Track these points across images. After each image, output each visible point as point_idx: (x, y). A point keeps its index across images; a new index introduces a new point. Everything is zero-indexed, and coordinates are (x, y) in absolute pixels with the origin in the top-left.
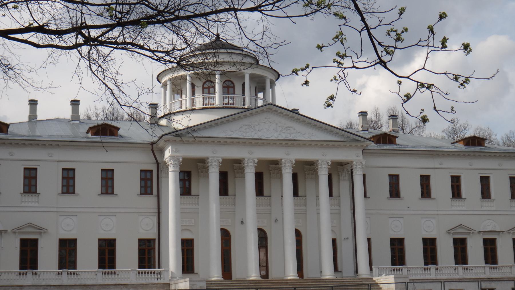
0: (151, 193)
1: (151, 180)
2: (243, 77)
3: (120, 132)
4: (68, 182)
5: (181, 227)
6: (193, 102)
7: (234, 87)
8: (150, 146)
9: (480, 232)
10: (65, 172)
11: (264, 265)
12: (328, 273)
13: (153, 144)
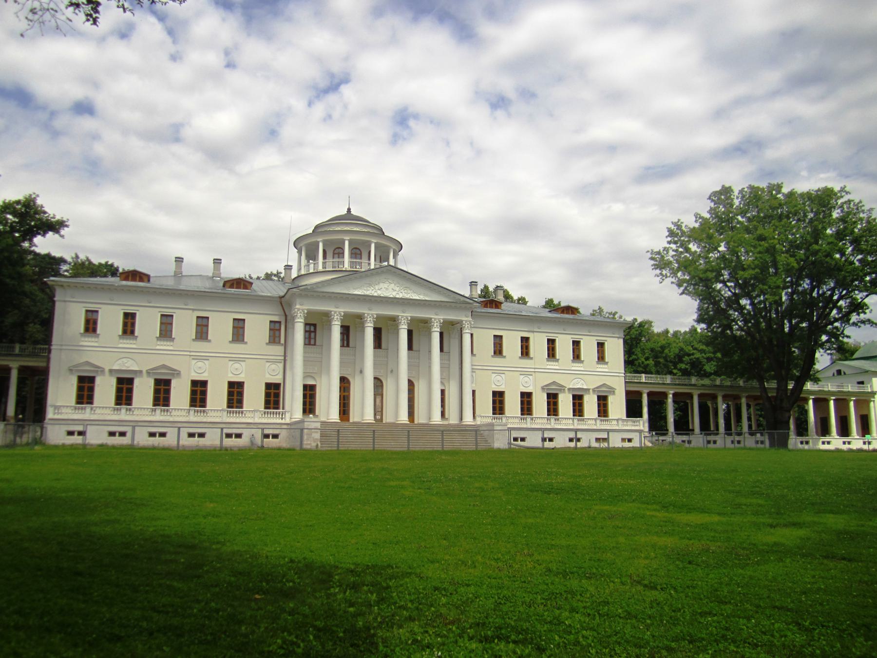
0: (279, 342)
1: (280, 330)
4: (274, 334)
7: (361, 254)
9: (569, 389)
10: (273, 324)
11: (378, 410)
12: (436, 418)
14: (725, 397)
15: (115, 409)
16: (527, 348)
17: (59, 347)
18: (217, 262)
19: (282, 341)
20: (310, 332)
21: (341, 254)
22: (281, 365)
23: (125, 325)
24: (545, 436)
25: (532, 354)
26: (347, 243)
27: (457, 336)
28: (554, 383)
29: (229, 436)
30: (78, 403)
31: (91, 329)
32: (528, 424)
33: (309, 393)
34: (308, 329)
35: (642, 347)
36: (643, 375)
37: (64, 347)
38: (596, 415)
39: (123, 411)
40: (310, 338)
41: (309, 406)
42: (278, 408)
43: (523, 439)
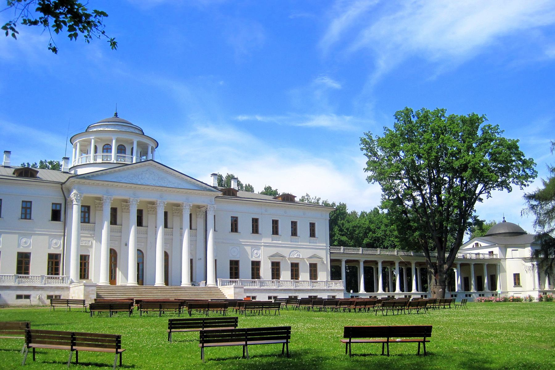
2: (132, 143)
3: (38, 175)
4: (26, 211)
5: (79, 246)
6: (95, 158)
7: (125, 150)
8: (60, 186)
10: (83, 208)
13: (62, 184)
16: (236, 225)
25: (239, 229)
26: (114, 141)
27: (203, 216)
33: (84, 261)
34: (24, 206)
35: (341, 225)
40: (26, 214)
41: (84, 273)
42: (58, 274)
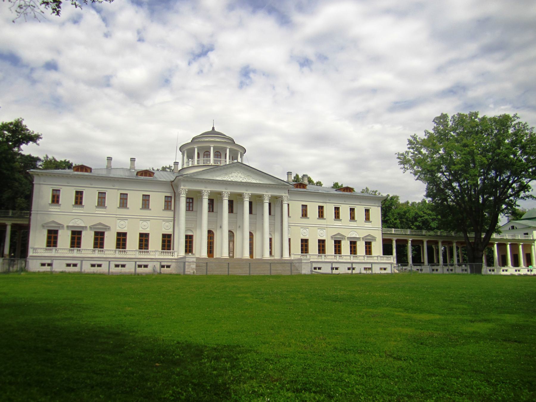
0: (171, 209)
1: (171, 202)
4: (168, 204)
7: (221, 155)
9: (348, 238)
10: (167, 198)
11: (231, 251)
12: (267, 256)
14: (443, 243)
15: (70, 250)
16: (322, 212)
17: (36, 212)
18: (133, 160)
19: (173, 208)
20: (189, 203)
21: (208, 155)
22: (172, 223)
23: (76, 198)
24: (333, 266)
25: (325, 216)
26: (212, 148)
27: (280, 205)
28: (339, 234)
29: (140, 266)
30: (48, 246)
31: (55, 201)
32: (323, 259)
33: (189, 240)
34: (188, 201)
35: (392, 212)
36: (393, 229)
37: (39, 212)
38: (364, 253)
39: (75, 251)
40: (189, 206)
41: (189, 248)
42: (170, 249)
43: (320, 268)
